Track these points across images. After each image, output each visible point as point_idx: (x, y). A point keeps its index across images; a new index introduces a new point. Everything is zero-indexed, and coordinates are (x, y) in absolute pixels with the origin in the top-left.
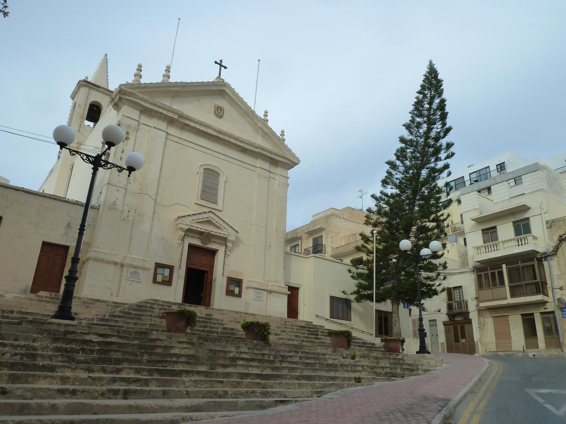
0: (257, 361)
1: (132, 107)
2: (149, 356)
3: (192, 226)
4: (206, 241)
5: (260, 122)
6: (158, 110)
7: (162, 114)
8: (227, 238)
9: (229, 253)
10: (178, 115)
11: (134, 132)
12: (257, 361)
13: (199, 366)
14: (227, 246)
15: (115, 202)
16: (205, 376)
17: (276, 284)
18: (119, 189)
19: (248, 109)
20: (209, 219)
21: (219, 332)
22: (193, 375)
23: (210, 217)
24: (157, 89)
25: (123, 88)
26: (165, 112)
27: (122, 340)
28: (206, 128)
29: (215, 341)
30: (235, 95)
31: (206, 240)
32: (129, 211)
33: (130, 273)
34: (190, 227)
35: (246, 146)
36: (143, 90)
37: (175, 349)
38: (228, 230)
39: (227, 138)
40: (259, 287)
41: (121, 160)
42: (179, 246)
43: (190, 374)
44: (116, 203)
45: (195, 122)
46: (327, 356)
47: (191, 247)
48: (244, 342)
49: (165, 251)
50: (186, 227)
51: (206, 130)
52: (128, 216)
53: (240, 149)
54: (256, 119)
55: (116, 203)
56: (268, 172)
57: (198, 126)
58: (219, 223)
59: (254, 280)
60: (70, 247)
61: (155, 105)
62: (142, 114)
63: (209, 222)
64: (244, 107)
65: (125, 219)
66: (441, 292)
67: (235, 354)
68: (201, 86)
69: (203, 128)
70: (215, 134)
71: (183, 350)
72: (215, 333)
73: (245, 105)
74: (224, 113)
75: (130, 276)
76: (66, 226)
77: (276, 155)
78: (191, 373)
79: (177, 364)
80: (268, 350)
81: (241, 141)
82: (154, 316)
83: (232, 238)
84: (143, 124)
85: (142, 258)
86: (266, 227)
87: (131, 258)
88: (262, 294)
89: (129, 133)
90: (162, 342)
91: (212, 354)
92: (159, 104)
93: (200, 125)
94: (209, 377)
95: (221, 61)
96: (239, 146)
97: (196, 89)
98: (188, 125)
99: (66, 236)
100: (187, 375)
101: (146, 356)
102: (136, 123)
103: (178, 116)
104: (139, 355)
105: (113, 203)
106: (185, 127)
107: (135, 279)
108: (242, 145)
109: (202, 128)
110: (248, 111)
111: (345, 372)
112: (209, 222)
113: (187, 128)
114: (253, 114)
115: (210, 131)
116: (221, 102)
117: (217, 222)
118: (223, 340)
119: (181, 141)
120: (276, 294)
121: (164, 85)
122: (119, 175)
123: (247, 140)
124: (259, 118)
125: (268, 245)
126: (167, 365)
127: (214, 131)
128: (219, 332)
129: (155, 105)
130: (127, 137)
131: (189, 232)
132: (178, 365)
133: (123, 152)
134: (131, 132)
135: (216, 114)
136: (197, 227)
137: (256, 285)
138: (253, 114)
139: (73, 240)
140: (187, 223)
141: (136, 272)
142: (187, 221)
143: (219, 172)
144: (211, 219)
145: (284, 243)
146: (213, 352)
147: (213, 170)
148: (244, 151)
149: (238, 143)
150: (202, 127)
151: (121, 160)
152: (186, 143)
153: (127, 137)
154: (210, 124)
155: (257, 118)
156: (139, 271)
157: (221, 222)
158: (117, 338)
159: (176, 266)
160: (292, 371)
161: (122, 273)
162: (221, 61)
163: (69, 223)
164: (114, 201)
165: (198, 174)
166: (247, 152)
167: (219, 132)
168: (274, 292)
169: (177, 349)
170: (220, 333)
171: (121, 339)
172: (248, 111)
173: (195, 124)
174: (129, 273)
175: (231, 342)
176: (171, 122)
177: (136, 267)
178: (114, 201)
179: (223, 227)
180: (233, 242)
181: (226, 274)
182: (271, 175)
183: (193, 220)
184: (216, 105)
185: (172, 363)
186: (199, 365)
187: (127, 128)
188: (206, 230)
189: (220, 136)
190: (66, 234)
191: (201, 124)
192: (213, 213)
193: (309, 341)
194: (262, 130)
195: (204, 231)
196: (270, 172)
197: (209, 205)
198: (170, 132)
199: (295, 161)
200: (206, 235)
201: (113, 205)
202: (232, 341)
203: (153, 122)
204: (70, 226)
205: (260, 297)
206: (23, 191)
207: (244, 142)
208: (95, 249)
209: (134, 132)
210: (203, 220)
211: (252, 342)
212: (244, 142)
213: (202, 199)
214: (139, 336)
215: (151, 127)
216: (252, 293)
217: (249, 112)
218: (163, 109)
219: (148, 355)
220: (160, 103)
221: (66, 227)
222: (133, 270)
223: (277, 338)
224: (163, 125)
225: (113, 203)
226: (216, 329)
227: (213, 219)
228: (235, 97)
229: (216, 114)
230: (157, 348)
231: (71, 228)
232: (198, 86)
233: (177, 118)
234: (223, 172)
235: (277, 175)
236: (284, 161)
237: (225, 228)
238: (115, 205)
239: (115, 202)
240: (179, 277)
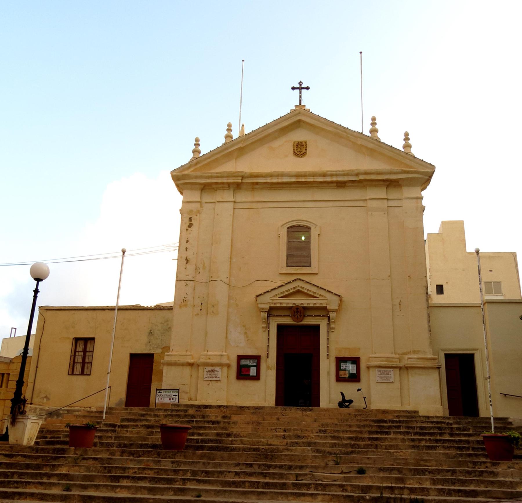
0: (149, 479)
1: (191, 189)
2: (19, 476)
3: (275, 303)
4: (297, 317)
5: (358, 138)
6: (217, 182)
7: (222, 183)
8: (327, 307)
9: (334, 326)
10: (240, 177)
11: (197, 216)
12: (149, 479)
13: (54, 487)
14: (329, 317)
15: (185, 298)
16: (39, 498)
17: (416, 356)
18: (188, 282)
19: (336, 128)
20: (297, 289)
21: (200, 441)
22: (26, 498)
23: (299, 286)
24: (213, 158)
25: (174, 174)
26: (225, 180)
27: (26, 459)
28: (280, 178)
29: (142, 454)
30: (315, 119)
31: (298, 316)
32: (202, 304)
33: (206, 373)
34: (272, 305)
35: (340, 179)
36: (196, 167)
37: (63, 467)
38: (326, 297)
39: (311, 179)
40: (384, 364)
41: (186, 251)
42: (264, 331)
43: (22, 496)
44: (186, 299)
45: (264, 177)
46: (308, 469)
47: (280, 327)
48: (183, 454)
49: (248, 340)
50: (267, 307)
51: (280, 181)
52: (201, 310)
53: (335, 185)
54: (351, 137)
55: (186, 299)
56: (386, 201)
57: (268, 180)
58: (311, 291)
59: (377, 355)
60: (154, 355)
61: (211, 177)
62: (205, 192)
63: (298, 292)
64: (330, 129)
65: (198, 314)
66: (4, 409)
67: (136, 470)
68: (266, 129)
69: (275, 179)
70: (294, 180)
71: (72, 468)
72: (195, 441)
73: (331, 126)
74: (308, 149)
75: (207, 376)
76: (148, 334)
77: (391, 173)
78: (24, 495)
79: (29, 485)
80: (201, 463)
81: (332, 175)
82: (140, 426)
83: (333, 304)
84: (206, 203)
85: (219, 353)
86: (390, 279)
87: (207, 355)
88: (390, 373)
89: (192, 219)
90: (66, 459)
91: (106, 471)
92: (215, 174)
93: (271, 178)
94: (43, 500)
95: (300, 83)
96: (332, 182)
97: (263, 136)
98: (257, 183)
99: (150, 344)
100: (19, 497)
101: (16, 476)
102: (198, 205)
103: (241, 178)
104: (9, 475)
105: (183, 300)
106: (254, 187)
107: (213, 378)
108: (334, 179)
109: (275, 180)
110: (338, 131)
111: (280, 496)
112: (298, 292)
113: (258, 186)
114: (346, 132)
115: (285, 180)
116: (299, 136)
117: (308, 290)
118: (153, 452)
119: (254, 205)
120: (416, 371)
121: (219, 150)
122: (186, 268)
123: (339, 171)
124: (355, 134)
125: (397, 302)
126: (18, 486)
127: (290, 178)
128: (200, 441)
129: (211, 177)
130: (190, 224)
131: (272, 312)
132: (30, 486)
133: (187, 241)
134: (193, 217)
135: (296, 154)
136: (281, 303)
137: (378, 363)
138: (346, 132)
139: (156, 346)
140: (267, 302)
141: (213, 371)
142: (267, 298)
143: (308, 225)
144: (300, 289)
145: (425, 294)
146: (107, 468)
147: (299, 226)
148: (341, 185)
149: (328, 179)
150: (274, 178)
151: (186, 251)
152: (259, 205)
153: (190, 224)
154: (283, 171)
155: (352, 135)
156: (217, 369)
157: (314, 289)
158: (21, 457)
159: (263, 355)
160: (180, 493)
161: (198, 374)
162: (300, 83)
163: (151, 330)
164: (184, 297)
165: (279, 236)
166: (346, 185)
167: (298, 175)
168: (412, 368)
169: (65, 467)
170: (201, 440)
171: (25, 459)
172: (338, 131)
173: (264, 178)
174: (205, 373)
175: (164, 455)
176: (237, 187)
177: (212, 365)
178: (184, 297)
179: (318, 294)
180: (337, 311)
181: (334, 354)
182: (391, 203)
183: (276, 295)
184: (294, 143)
185: (24, 483)
186: (53, 486)
187: (189, 214)
188: (294, 304)
189: (300, 180)
190: (150, 342)
191: (271, 175)
192: (301, 280)
193: (347, 444)
194: (366, 147)
195: (291, 305)
196: (388, 199)
197: (299, 271)
198: (237, 200)
199: (427, 170)
200: (296, 310)
201: (183, 302)
202: (166, 453)
203: (220, 195)
204: (151, 333)
205: (388, 379)
206: (108, 309)
207: (336, 175)
208: (170, 353)
209: (197, 216)
210: (288, 293)
211: (194, 454)
212: (336, 175)
213: (289, 266)
214: (372, 429)
215: (215, 202)
216: (374, 375)
217: (340, 132)
218: (222, 177)
219: (18, 476)
220: (217, 173)
221: (148, 335)
222: (209, 368)
223: (287, 443)
224: (228, 195)
225: (183, 300)
226: (206, 436)
227: (302, 287)
228: (316, 122)
229: (296, 154)
230: (44, 467)
231: (153, 335)
232: (262, 131)
233: (240, 181)
234: (314, 224)
235: (402, 199)
236: (415, 176)
237: (320, 295)
238: (185, 301)
239: (185, 298)
240: (268, 368)
